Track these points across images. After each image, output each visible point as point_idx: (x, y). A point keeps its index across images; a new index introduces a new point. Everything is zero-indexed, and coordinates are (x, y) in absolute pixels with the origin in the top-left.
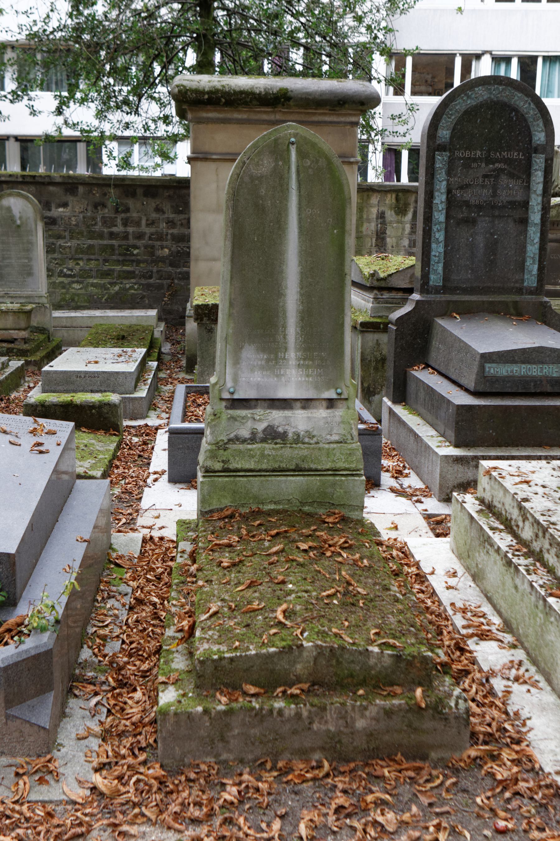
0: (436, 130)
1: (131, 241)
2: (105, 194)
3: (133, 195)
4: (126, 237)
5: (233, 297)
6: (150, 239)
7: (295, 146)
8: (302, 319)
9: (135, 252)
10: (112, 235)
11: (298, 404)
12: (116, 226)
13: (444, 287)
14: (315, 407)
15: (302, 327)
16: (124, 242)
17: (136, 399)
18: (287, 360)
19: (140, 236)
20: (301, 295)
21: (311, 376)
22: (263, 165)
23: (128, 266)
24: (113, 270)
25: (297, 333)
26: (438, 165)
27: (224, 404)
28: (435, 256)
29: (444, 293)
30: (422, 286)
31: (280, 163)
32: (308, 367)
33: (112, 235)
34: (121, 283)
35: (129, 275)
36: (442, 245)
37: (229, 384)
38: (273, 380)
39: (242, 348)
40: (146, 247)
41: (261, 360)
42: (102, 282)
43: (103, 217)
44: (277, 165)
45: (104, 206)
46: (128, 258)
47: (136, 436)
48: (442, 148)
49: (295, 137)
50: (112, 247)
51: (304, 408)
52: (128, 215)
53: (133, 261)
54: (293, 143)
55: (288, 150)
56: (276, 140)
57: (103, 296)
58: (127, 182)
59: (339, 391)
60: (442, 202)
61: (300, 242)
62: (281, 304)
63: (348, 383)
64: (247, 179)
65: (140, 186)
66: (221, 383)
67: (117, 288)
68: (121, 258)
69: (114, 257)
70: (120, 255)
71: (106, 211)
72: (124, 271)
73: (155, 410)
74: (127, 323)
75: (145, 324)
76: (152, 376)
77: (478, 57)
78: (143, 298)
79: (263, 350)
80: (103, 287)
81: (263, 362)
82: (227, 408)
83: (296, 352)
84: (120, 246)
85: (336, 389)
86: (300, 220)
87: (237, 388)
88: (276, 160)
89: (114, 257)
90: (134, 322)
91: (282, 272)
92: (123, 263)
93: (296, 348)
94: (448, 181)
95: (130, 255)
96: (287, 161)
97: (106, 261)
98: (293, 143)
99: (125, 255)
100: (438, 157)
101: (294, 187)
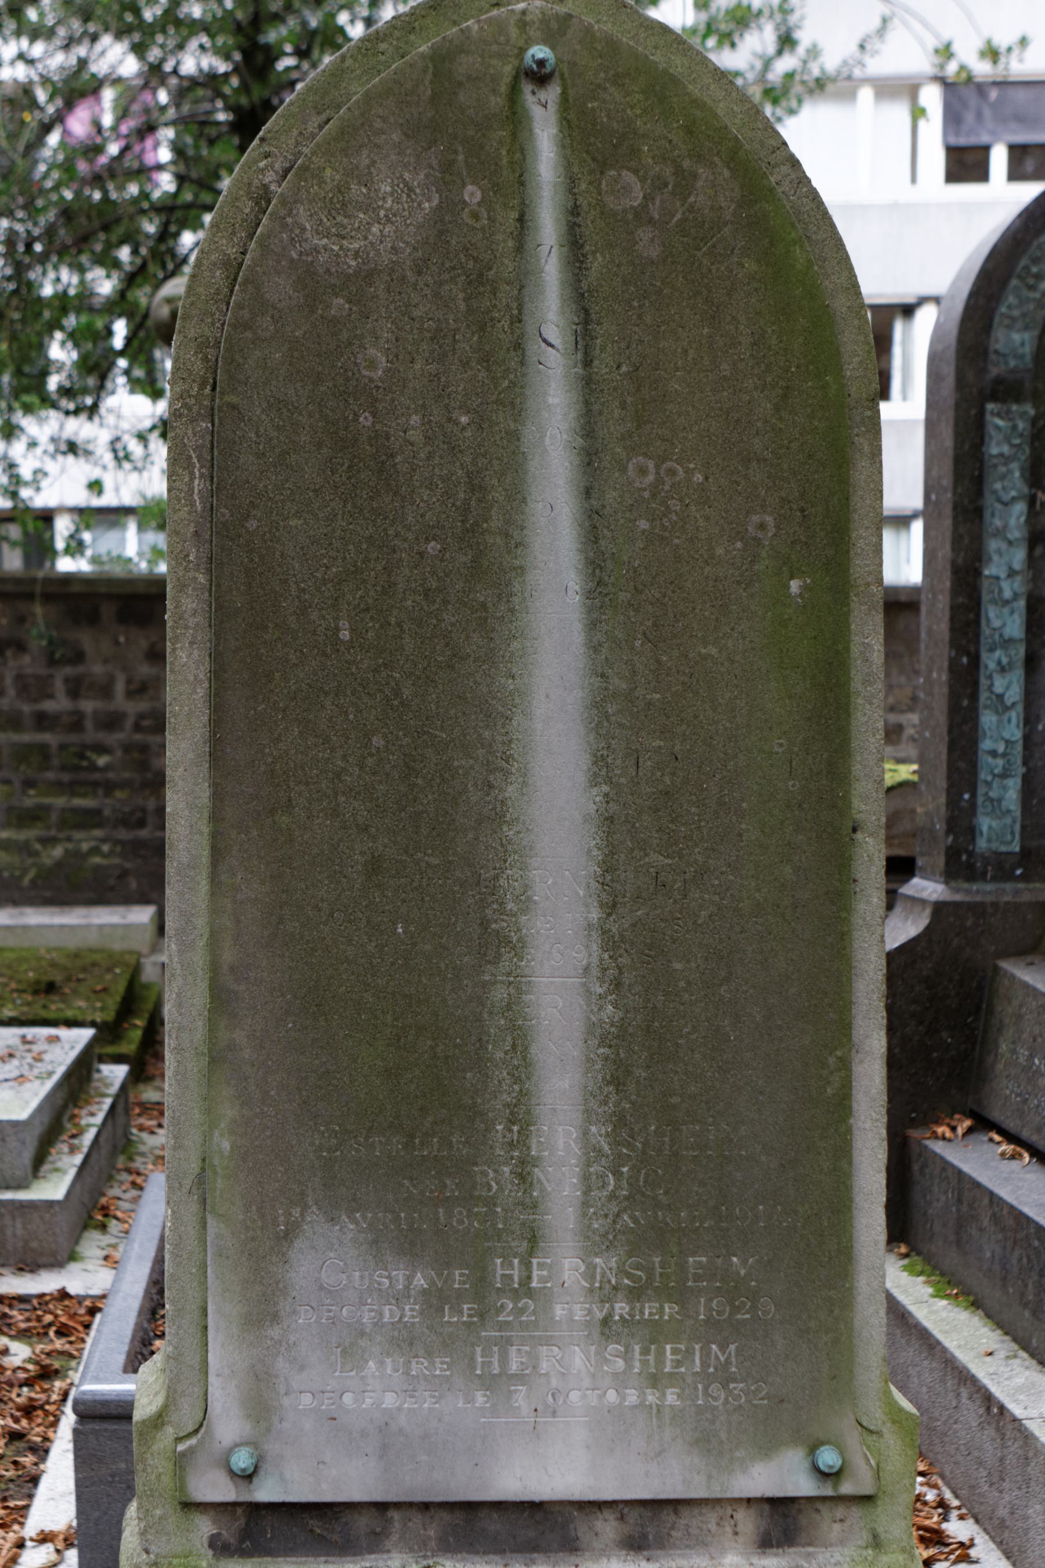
0: (987, 328)
1: (91, 735)
2: (21, 620)
3: (93, 619)
4: (76, 724)
5: (228, 956)
6: (137, 728)
7: (552, 93)
8: (617, 1077)
9: (102, 761)
10: (43, 721)
11: (607, 1527)
12: (51, 697)
13: (1026, 855)
14: (701, 1542)
15: (619, 1121)
16: (73, 738)
17: (32, 1205)
18: (543, 1298)
19: (111, 722)
20: (611, 943)
21: (673, 1378)
22: (368, 207)
23: (84, 795)
24: (47, 809)
25: (591, 1154)
26: (995, 448)
27: (205, 1527)
28: (994, 754)
29: (1025, 878)
30: (952, 855)
31: (472, 194)
32: (655, 1334)
33: (43, 721)
34: (69, 839)
35: (89, 819)
36: (1015, 716)
37: (228, 1426)
38: (463, 1407)
39: (288, 1236)
40: (127, 748)
41: (399, 1299)
42: (22, 836)
43: (19, 678)
44: (451, 206)
45: (21, 647)
46: (83, 776)
47: (23, 1335)
48: (1006, 390)
49: (549, 40)
50: (43, 749)
51: (635, 1544)
52: (81, 669)
53: (95, 784)
54: (540, 76)
55: (516, 120)
56: (441, 60)
57: (25, 871)
58: (75, 588)
59: (828, 1458)
60: (1012, 573)
61: (594, 648)
62: (499, 994)
63: (875, 1415)
64: (281, 289)
65: (110, 597)
66: (186, 1416)
67: (58, 852)
68: (66, 777)
69: (50, 775)
70: (63, 768)
71: (27, 659)
72: (75, 811)
73: (103, 1227)
74: (72, 943)
75: (117, 946)
76: (99, 1119)
77: (908, 311)
78: (124, 874)
79: (409, 1245)
80: (24, 848)
81: (411, 1312)
82: (219, 1547)
83: (587, 1254)
84: (62, 747)
85: (813, 1449)
86: (594, 526)
87: (272, 1448)
88: (447, 177)
89: (50, 775)
90: (93, 940)
91: (497, 817)
92: (71, 789)
93: (586, 1232)
94: (1032, 501)
95: (87, 769)
96: (513, 183)
97: (29, 784)
98: (540, 76)
99: (77, 768)
100: (996, 422)
101: (552, 333)
